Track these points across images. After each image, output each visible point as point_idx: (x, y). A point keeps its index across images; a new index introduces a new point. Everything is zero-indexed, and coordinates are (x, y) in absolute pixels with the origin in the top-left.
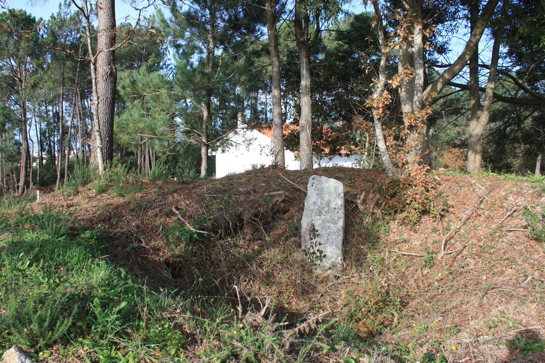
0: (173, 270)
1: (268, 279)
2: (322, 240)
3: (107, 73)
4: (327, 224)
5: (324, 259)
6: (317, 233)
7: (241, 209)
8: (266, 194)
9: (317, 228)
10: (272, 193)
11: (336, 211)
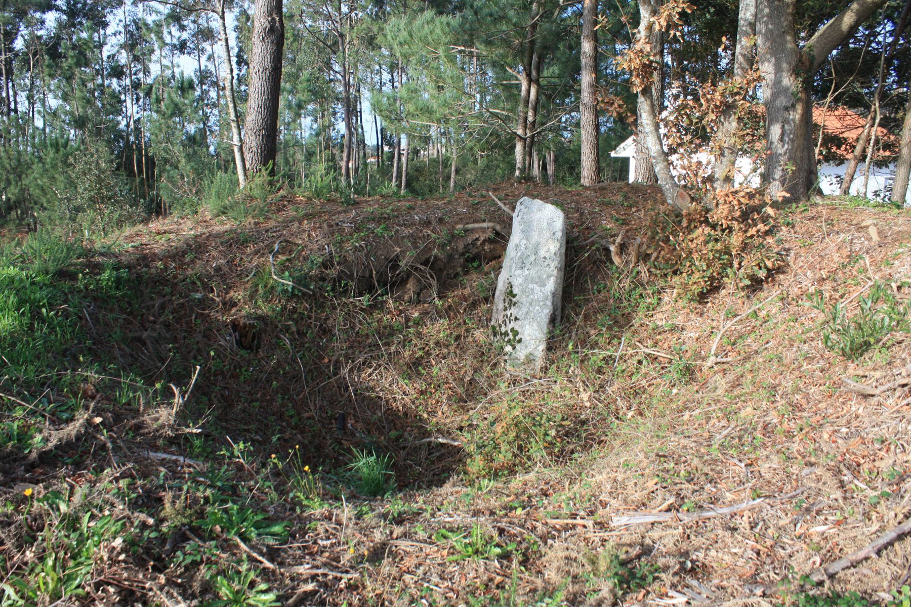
0: (241, 337)
1: (415, 368)
3: (265, 30)
4: (531, 286)
5: (518, 346)
6: (514, 300)
7: (399, 250)
8: (460, 226)
9: (515, 291)
10: (470, 226)
11: (546, 263)
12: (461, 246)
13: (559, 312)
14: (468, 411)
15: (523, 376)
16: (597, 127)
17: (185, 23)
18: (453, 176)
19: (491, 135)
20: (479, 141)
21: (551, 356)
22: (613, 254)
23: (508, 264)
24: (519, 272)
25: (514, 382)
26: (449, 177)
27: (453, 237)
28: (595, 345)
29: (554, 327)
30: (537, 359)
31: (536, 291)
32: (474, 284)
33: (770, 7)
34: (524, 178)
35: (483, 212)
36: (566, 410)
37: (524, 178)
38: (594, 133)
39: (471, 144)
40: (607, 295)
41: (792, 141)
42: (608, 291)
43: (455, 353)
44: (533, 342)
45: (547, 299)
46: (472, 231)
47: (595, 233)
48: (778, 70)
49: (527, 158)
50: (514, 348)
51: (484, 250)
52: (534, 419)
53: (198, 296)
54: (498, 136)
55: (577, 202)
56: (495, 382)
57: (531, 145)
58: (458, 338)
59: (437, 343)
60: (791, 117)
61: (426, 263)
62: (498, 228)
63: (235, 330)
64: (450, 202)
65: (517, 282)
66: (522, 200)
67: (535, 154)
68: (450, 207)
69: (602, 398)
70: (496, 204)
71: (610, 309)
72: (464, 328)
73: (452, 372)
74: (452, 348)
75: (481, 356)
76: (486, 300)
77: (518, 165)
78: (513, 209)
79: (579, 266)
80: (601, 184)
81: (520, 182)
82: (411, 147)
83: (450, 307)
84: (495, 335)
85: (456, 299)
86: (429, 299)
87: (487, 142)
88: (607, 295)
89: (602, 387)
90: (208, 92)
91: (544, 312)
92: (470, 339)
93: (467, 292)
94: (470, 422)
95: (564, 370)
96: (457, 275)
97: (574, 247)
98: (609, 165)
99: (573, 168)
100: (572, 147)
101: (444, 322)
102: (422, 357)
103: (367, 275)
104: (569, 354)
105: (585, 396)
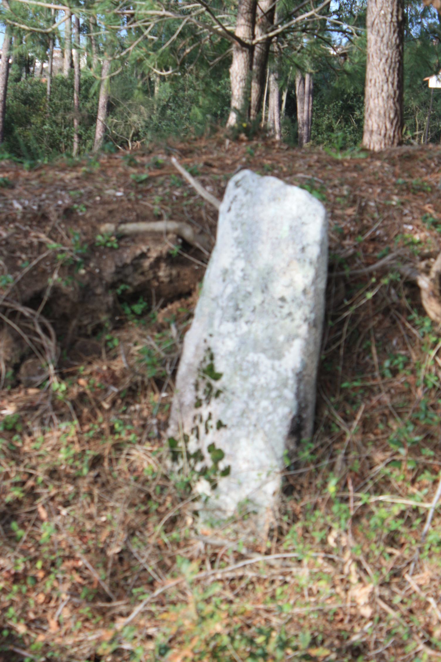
2: (229, 412)
5: (223, 483)
6: (217, 385)
8: (108, 227)
9: (220, 366)
11: (285, 311)
12: (109, 271)
13: (309, 414)
14: (113, 619)
15: (231, 546)
16: (401, 25)
18: (101, 116)
19: (182, 35)
20: (156, 47)
21: (291, 505)
22: (424, 295)
23: (206, 310)
24: (229, 326)
25: (214, 558)
26: (93, 119)
27: (93, 249)
28: (382, 486)
29: (298, 443)
30: (262, 511)
31: (262, 368)
32: (135, 350)
34: (246, 131)
35: (157, 199)
36: (321, 623)
37: (246, 131)
38: (394, 39)
39: (140, 53)
40: (411, 379)
42: (413, 372)
43: (90, 494)
44: (254, 474)
45: (285, 385)
47: (390, 251)
49: (255, 86)
50: (214, 487)
51: (156, 278)
52: (251, 641)
54: (196, 38)
55: (353, 184)
56: (173, 559)
57: (262, 63)
58: (96, 462)
59: (53, 473)
61: (33, 302)
62: (188, 232)
64: (89, 176)
65: (225, 348)
66: (238, 177)
67: (271, 78)
68: (90, 187)
69: (397, 600)
70: (185, 184)
71: (417, 410)
72: (109, 443)
73: (81, 535)
74: (84, 485)
75: (144, 502)
76: (159, 383)
77: (236, 103)
78: (220, 194)
79: (354, 318)
80: (405, 148)
81: (237, 139)
82: (15, 52)
83: (82, 396)
84: (175, 458)
85: (96, 380)
86: (39, 379)
87: (173, 49)
88: (411, 379)
89: (396, 574)
91: (278, 412)
92: (122, 465)
93: (119, 364)
94: (115, 646)
95: (318, 536)
96: (99, 328)
97: (344, 278)
98: (424, 104)
99: (351, 109)
100: (348, 67)
101: (70, 428)
102: (18, 502)
104: (330, 502)
105: (360, 594)
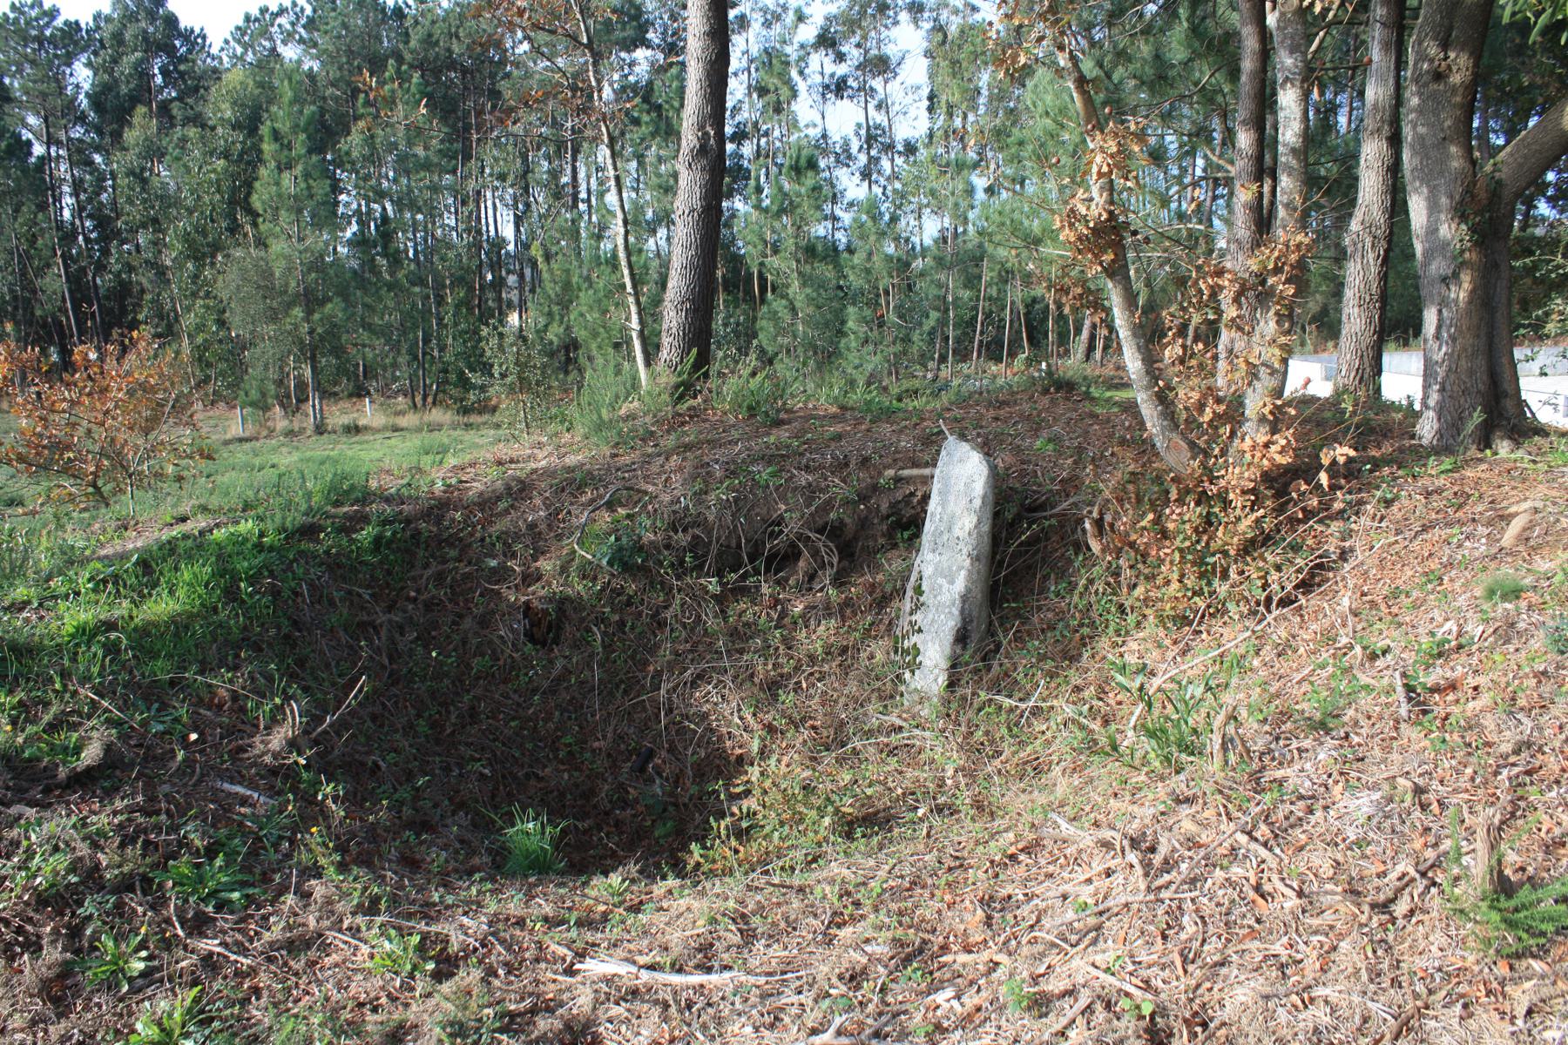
0: (532, 625)
8: (890, 472)
17: (844, 49)
33: (1420, 94)
41: (1453, 339)
46: (908, 480)
48: (1433, 207)
53: (493, 563)
60: (1453, 295)
61: (820, 531)
63: (526, 616)
90: (878, 160)
103: (734, 544)
